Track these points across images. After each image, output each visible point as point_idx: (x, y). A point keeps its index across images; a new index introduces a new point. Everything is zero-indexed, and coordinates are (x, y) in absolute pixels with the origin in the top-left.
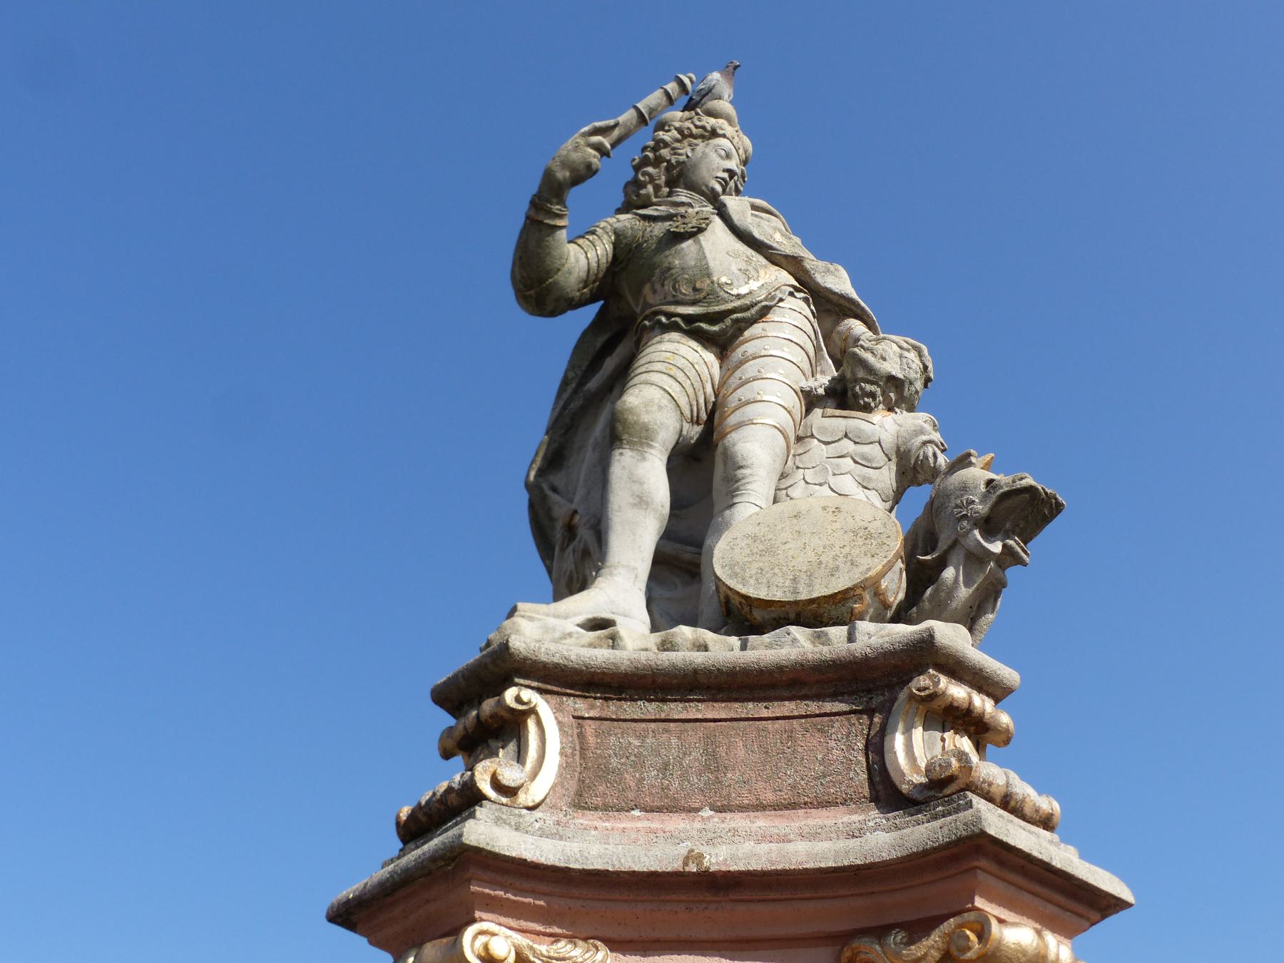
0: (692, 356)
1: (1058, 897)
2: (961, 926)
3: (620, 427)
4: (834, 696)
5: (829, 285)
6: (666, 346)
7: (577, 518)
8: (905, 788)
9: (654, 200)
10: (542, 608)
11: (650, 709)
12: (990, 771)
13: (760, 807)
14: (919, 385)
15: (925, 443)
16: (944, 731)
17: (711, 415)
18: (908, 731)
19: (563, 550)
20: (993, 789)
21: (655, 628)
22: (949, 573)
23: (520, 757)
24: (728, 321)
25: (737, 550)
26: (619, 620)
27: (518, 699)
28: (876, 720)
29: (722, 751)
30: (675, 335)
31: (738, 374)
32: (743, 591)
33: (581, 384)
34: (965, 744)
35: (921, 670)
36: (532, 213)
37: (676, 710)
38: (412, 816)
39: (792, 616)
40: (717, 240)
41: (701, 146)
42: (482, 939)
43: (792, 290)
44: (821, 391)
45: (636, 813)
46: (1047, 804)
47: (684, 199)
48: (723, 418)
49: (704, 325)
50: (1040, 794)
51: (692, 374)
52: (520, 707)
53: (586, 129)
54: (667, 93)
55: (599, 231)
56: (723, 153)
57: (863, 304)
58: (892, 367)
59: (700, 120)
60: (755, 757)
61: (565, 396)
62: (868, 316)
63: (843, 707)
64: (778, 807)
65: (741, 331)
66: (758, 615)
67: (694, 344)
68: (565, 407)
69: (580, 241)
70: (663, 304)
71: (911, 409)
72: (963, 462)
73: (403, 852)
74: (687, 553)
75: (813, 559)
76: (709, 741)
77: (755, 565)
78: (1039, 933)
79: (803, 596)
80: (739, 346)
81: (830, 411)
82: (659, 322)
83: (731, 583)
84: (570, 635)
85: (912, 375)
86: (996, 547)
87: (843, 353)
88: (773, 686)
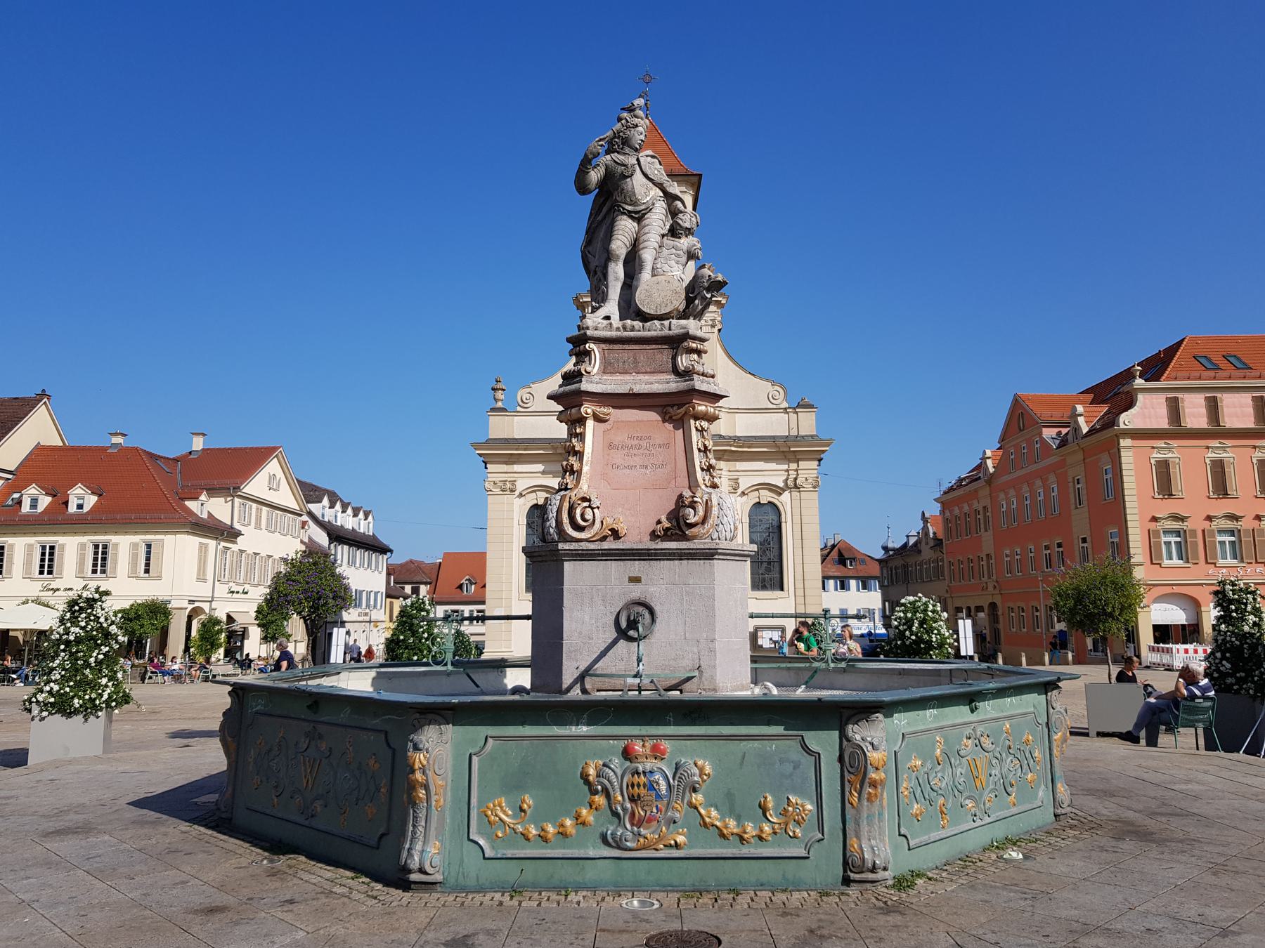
4: (665, 344)
6: (623, 222)
11: (621, 346)
13: (646, 373)
18: (681, 356)
22: (697, 302)
27: (589, 347)
30: (625, 217)
37: (626, 346)
40: (638, 176)
49: (634, 215)
53: (597, 139)
58: (687, 225)
61: (590, 222)
63: (667, 347)
64: (650, 373)
70: (623, 203)
79: (658, 313)
81: (669, 238)
83: (640, 307)
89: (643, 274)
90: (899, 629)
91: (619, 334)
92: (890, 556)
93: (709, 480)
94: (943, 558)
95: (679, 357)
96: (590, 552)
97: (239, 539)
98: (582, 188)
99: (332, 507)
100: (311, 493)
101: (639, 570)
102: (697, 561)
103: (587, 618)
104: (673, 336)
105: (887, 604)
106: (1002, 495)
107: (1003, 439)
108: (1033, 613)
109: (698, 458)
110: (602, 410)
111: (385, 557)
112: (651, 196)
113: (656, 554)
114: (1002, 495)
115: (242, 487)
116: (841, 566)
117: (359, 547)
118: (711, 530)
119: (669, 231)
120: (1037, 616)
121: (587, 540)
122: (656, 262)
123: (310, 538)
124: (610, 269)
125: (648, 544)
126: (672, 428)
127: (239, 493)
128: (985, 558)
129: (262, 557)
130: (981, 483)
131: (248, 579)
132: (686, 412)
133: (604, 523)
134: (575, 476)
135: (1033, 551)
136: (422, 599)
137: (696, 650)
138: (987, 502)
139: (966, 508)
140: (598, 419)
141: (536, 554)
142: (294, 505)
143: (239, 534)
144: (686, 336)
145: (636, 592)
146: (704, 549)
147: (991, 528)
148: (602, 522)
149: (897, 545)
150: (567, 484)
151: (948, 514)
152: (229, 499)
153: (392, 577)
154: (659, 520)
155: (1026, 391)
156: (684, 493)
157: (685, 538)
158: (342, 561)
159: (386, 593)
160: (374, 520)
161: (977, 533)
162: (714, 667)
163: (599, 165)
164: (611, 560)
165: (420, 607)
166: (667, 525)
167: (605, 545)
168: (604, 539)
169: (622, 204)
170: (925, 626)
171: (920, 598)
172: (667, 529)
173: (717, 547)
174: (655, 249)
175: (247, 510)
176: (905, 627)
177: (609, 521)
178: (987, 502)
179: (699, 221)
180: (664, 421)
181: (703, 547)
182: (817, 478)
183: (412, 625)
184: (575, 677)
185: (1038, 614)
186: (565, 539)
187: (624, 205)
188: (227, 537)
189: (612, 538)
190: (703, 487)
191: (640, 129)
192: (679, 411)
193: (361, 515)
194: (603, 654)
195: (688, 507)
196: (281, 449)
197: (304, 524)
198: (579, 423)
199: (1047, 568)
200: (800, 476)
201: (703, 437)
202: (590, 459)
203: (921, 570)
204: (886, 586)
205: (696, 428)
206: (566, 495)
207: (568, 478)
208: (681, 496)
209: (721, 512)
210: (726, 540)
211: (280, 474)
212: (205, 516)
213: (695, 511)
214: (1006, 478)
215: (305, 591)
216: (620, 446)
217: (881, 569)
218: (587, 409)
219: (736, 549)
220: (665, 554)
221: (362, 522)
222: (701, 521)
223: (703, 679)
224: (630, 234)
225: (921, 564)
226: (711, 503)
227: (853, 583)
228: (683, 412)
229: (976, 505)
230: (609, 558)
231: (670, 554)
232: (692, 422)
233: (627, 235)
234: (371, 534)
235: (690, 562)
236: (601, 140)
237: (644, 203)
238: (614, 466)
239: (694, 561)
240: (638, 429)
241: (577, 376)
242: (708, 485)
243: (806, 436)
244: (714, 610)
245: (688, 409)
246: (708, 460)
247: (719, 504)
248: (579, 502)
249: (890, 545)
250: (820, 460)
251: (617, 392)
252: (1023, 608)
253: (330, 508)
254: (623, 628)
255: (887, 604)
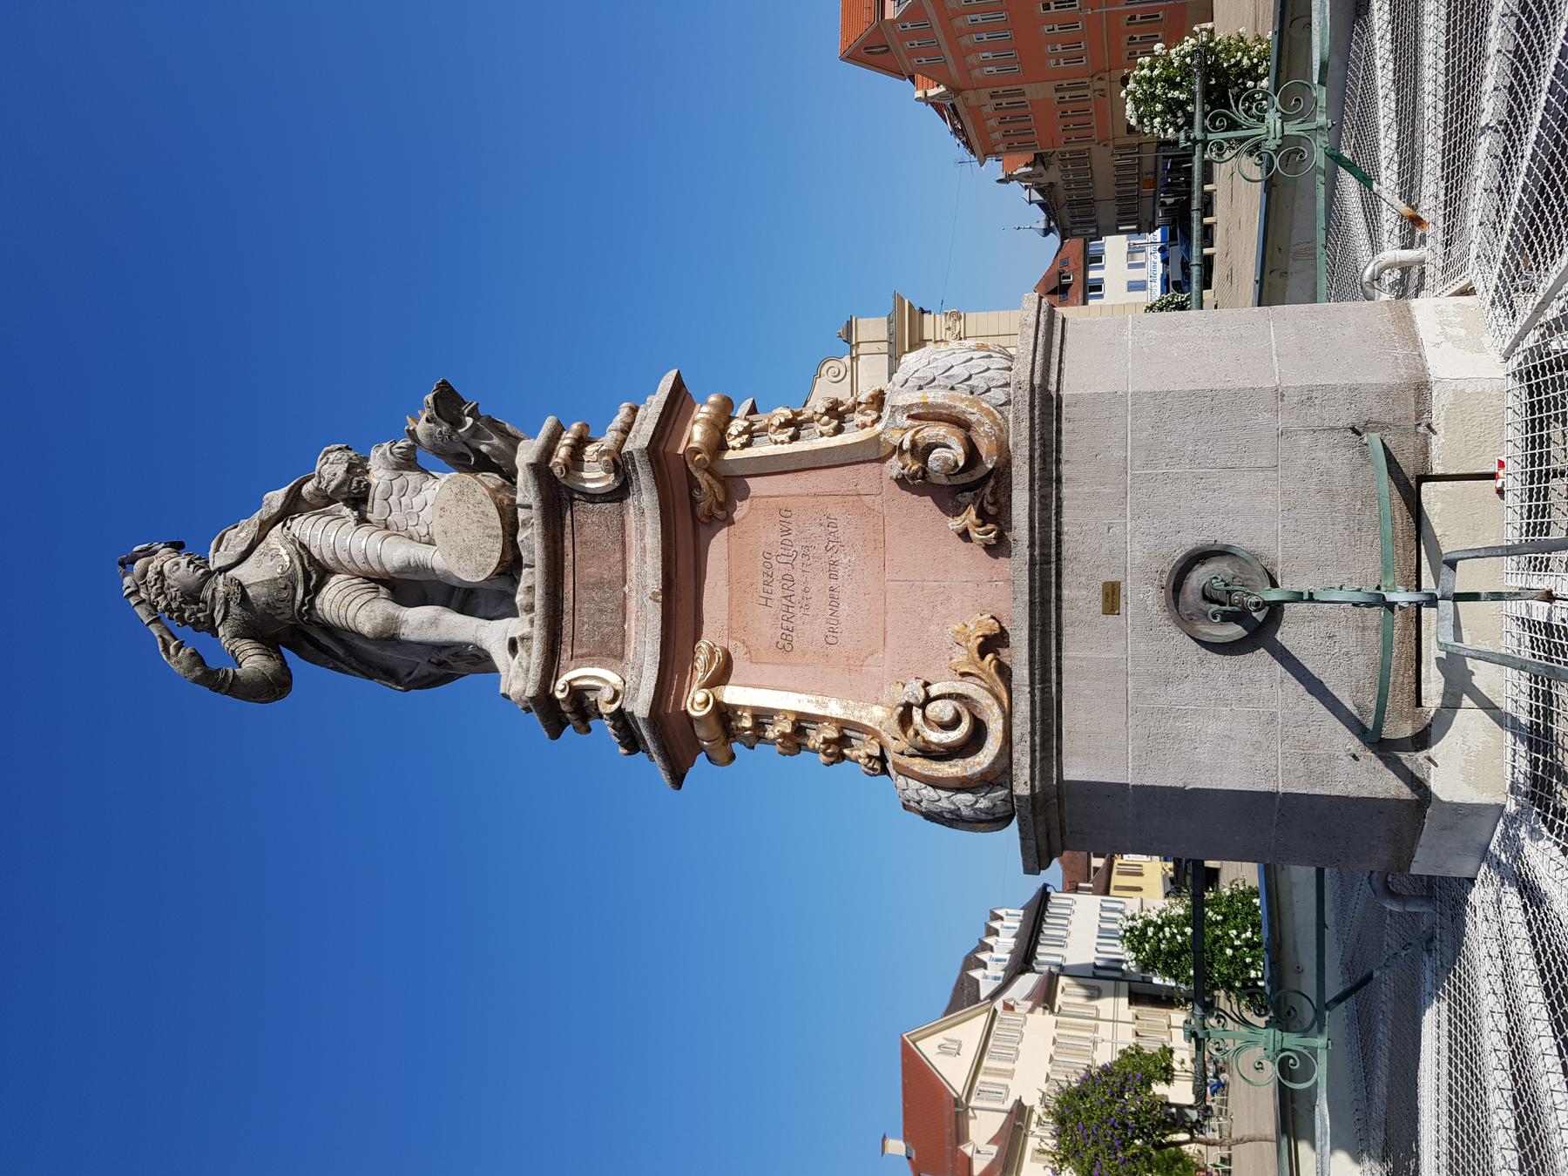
0: (334, 591)
1: (676, 409)
2: (693, 461)
3: (385, 635)
4: (562, 518)
5: (279, 504)
6: (326, 607)
7: (433, 660)
8: (617, 484)
9: (208, 612)
10: (503, 679)
11: (567, 618)
12: (608, 440)
13: (624, 561)
14: (352, 454)
15: (392, 453)
16: (583, 461)
17: (371, 580)
18: (584, 480)
19: (452, 668)
20: (619, 438)
21: (516, 615)
22: (484, 448)
23: (596, 689)
24: (310, 569)
25: (467, 568)
26: (510, 635)
27: (563, 691)
28: (576, 496)
29: (592, 580)
30: (318, 601)
31: (345, 564)
32: (495, 565)
33: (337, 658)
34: (590, 449)
35: (551, 470)
36: (223, 691)
37: (568, 605)
38: (625, 747)
39: (511, 538)
40: (244, 573)
41: (169, 582)
42: (695, 706)
43: (285, 528)
44: (356, 513)
45: (626, 627)
46: (624, 410)
47: (210, 593)
48: (375, 572)
50: (618, 413)
51: (346, 591)
52: (568, 689)
53: (164, 656)
54: (137, 604)
55: (232, 648)
56: (175, 568)
57: (292, 484)
58: (341, 470)
59: (150, 582)
60: (596, 562)
61: (346, 668)
62: (299, 481)
63: (569, 513)
64: (624, 552)
65: (316, 560)
66: (509, 557)
67: (325, 590)
68: (354, 669)
69: (240, 660)
70: (293, 604)
71: (367, 459)
72: (412, 434)
73: (647, 751)
74: (458, 596)
75: (476, 525)
76: (586, 587)
77: (478, 558)
78: (695, 422)
79: (501, 532)
80: (325, 561)
81: (369, 509)
82: (306, 611)
83: (489, 572)
84: (520, 663)
85: (346, 457)
86: (469, 421)
87: (325, 500)
88: (555, 551)
89: (435, 565)
90: (1183, 126)
91: (537, 622)
92: (1057, 225)
93: (862, 413)
94: (1061, 153)
95: (588, 485)
96: (1038, 713)
97: (1026, 1102)
98: (275, 687)
99: (984, 965)
100: (964, 996)
101: (1087, 587)
102: (1064, 438)
103: (1213, 728)
104: (542, 500)
105: (1121, 228)
106: (976, 73)
107: (898, 74)
108: (1136, 24)
109: (811, 442)
110: (702, 668)
111: (1053, 894)
112: (280, 547)
113: (1045, 544)
114: (976, 73)
115: (956, 1096)
116: (1070, 291)
117: (1040, 931)
118: (984, 405)
119: (355, 508)
120: (1141, 18)
121: (1008, 717)
122: (416, 536)
123: (1027, 998)
124: (414, 637)
125: (1018, 564)
126: (746, 504)
127: (963, 1099)
128: (1061, 94)
129: (1052, 1070)
130: (958, 102)
131: (1087, 1053)
132: (706, 470)
133: (967, 670)
134: (852, 734)
135: (1051, 27)
136: (1126, 931)
137: (1305, 440)
138: (984, 93)
139: (993, 123)
140: (722, 675)
141: (1043, 843)
142: (981, 1021)
143: (1019, 1103)
144: (541, 469)
145: (1144, 597)
146: (1032, 419)
147: (1019, 87)
148: (963, 674)
149: (1042, 216)
150: (870, 757)
151: (1001, 148)
152: (971, 1113)
153: (1081, 885)
154: (959, 535)
155: (837, 46)
156: (895, 473)
157: (1002, 472)
158: (1058, 955)
159: (1102, 895)
160: (1001, 908)
161: (1027, 106)
162: (1353, 389)
163: (233, 652)
164: (1059, 658)
165: (1139, 935)
166: (970, 516)
167: (1021, 673)
168: (1004, 672)
169: (296, 608)
170: (1178, 79)
171: (1127, 94)
172: (983, 516)
173: (1027, 386)
174: (387, 536)
175: (986, 1089)
176: (1180, 114)
177: (963, 657)
178: (984, 93)
179: (338, 446)
180: (729, 521)
181: (1026, 424)
182: (946, 314)
183: (1170, 953)
184: (1379, 764)
185: (1138, 16)
186: (1004, 772)
187: (298, 603)
188: (1023, 1122)
189: (1004, 652)
190: (879, 427)
191: (167, 567)
192: (704, 485)
193: (996, 925)
194: (1315, 687)
195: (925, 463)
196: (905, 1035)
197: (1008, 1007)
198: (730, 720)
199: (1075, 5)
200: (943, 338)
201: (765, 429)
202: (813, 698)
203: (1076, 182)
204: (1097, 230)
205: (744, 446)
206: (895, 764)
207: (856, 753)
208: (902, 482)
209: (940, 381)
210: (1010, 369)
211: (938, 1039)
212: (994, 1149)
213: (937, 446)
214: (953, 71)
215: (1112, 1149)
216: (785, 624)
217: (1073, 236)
218: (696, 702)
219: (1032, 341)
220: (1045, 522)
221: (1006, 923)
222: (960, 432)
223: (1388, 419)
224: (346, 591)
225: (1068, 182)
226: (917, 405)
227: (1092, 274)
228: (706, 475)
229: (988, 109)
230: (1054, 665)
231: (1045, 507)
232: (729, 455)
233: (350, 598)
234: (1021, 912)
235: (1064, 456)
236: (166, 650)
237: (291, 561)
238: (830, 640)
239: (1064, 445)
240: (748, 581)
241: (626, 723)
242: (875, 416)
243: (889, 330)
244: (1194, 392)
245: (698, 465)
246: (817, 417)
247: (920, 388)
248: (911, 732)
249: (1042, 225)
250: (923, 312)
251: (658, 631)
252: (1130, 19)
253: (986, 968)
254: (1245, 633)
255: (1121, 228)
